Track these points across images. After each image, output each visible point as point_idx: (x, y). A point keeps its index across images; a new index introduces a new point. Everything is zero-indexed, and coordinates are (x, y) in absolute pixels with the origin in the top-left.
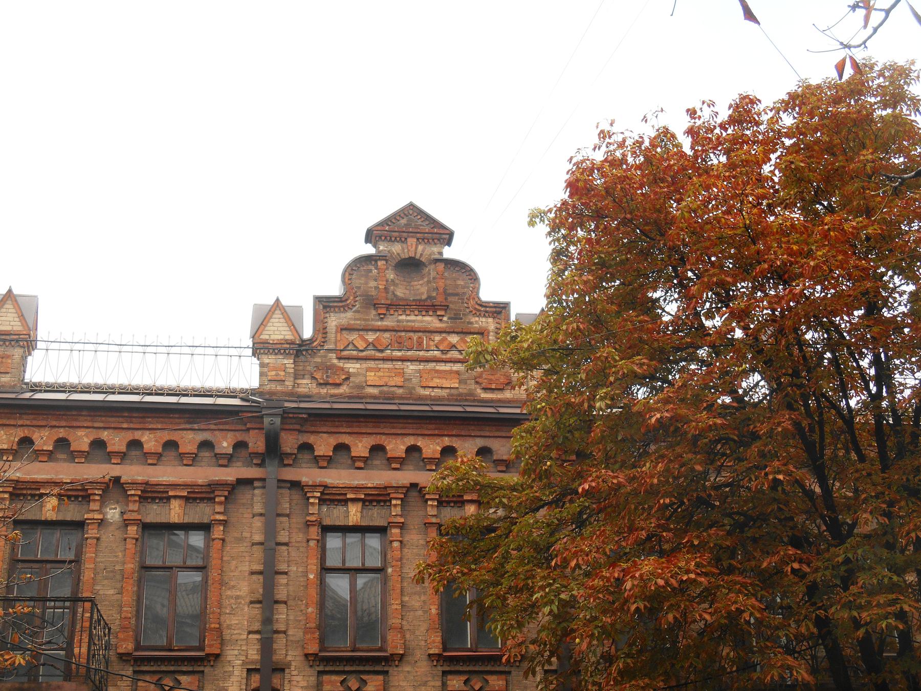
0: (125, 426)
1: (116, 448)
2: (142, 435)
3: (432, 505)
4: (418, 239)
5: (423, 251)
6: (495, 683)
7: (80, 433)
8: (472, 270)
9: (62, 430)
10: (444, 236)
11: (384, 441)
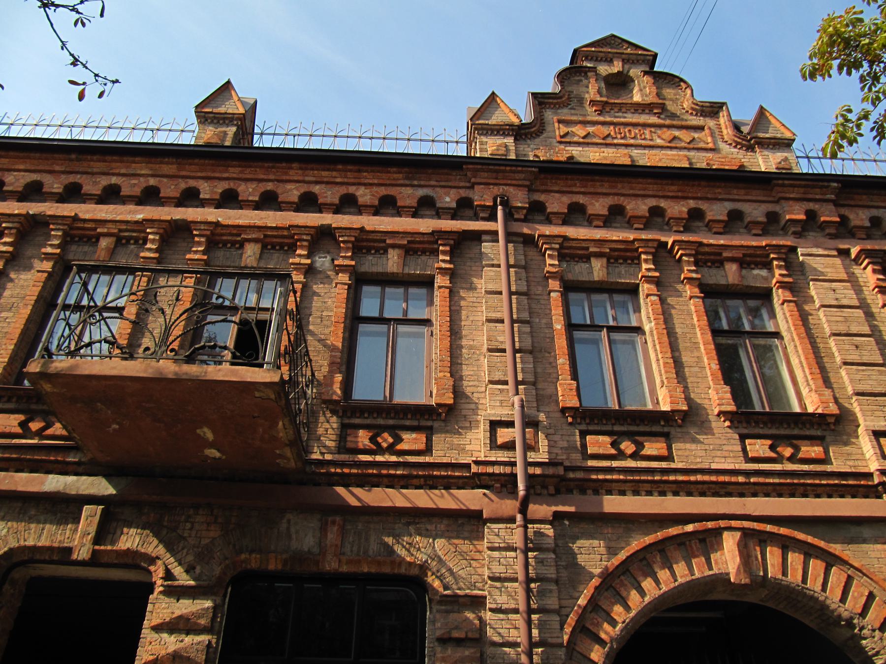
0: (338, 180)
1: (329, 200)
2: (357, 189)
3: (688, 261)
4: (623, 60)
7: (289, 186)
9: (270, 184)
10: (648, 57)
11: (623, 202)
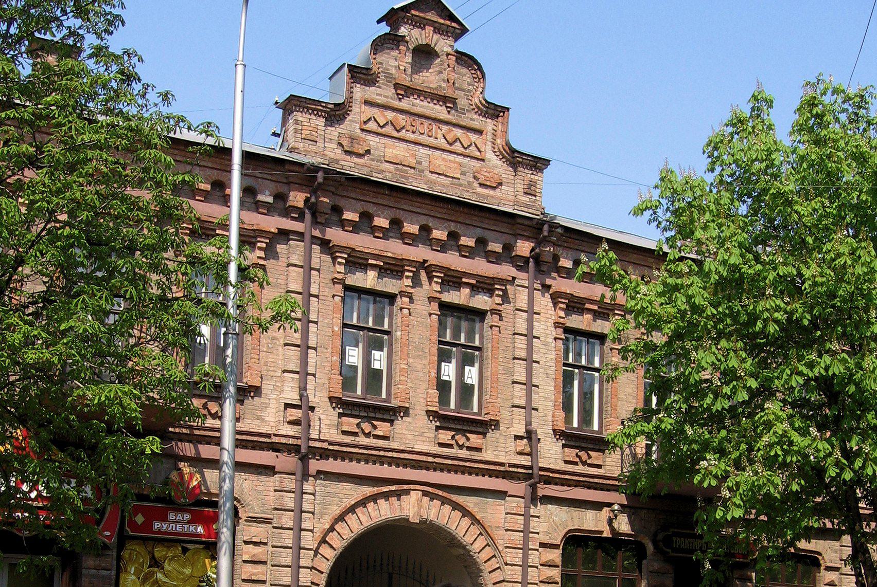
5: (438, 41)
8: (480, 68)
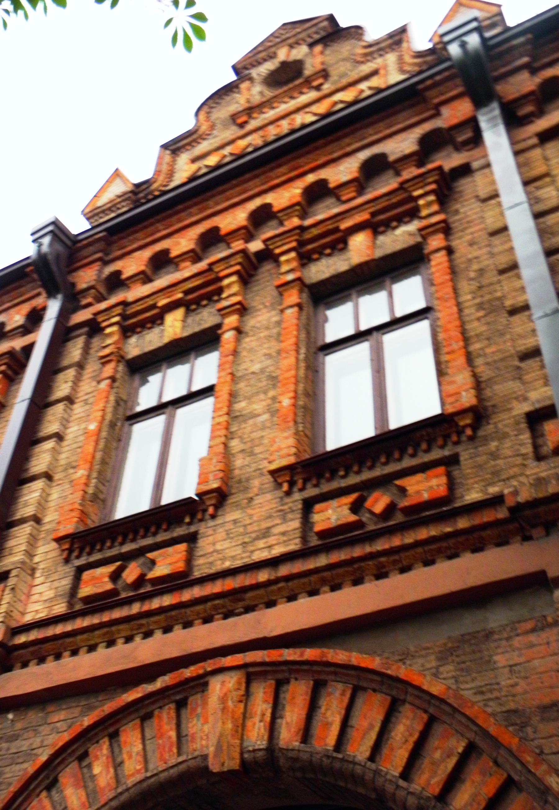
6: (421, 487)
